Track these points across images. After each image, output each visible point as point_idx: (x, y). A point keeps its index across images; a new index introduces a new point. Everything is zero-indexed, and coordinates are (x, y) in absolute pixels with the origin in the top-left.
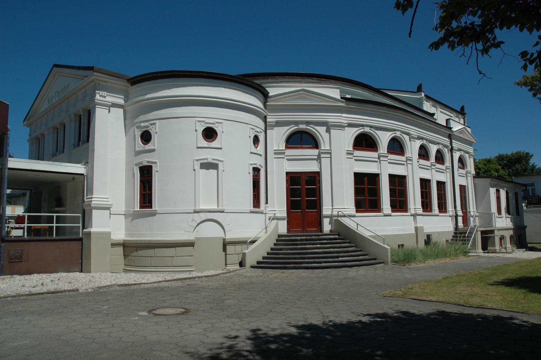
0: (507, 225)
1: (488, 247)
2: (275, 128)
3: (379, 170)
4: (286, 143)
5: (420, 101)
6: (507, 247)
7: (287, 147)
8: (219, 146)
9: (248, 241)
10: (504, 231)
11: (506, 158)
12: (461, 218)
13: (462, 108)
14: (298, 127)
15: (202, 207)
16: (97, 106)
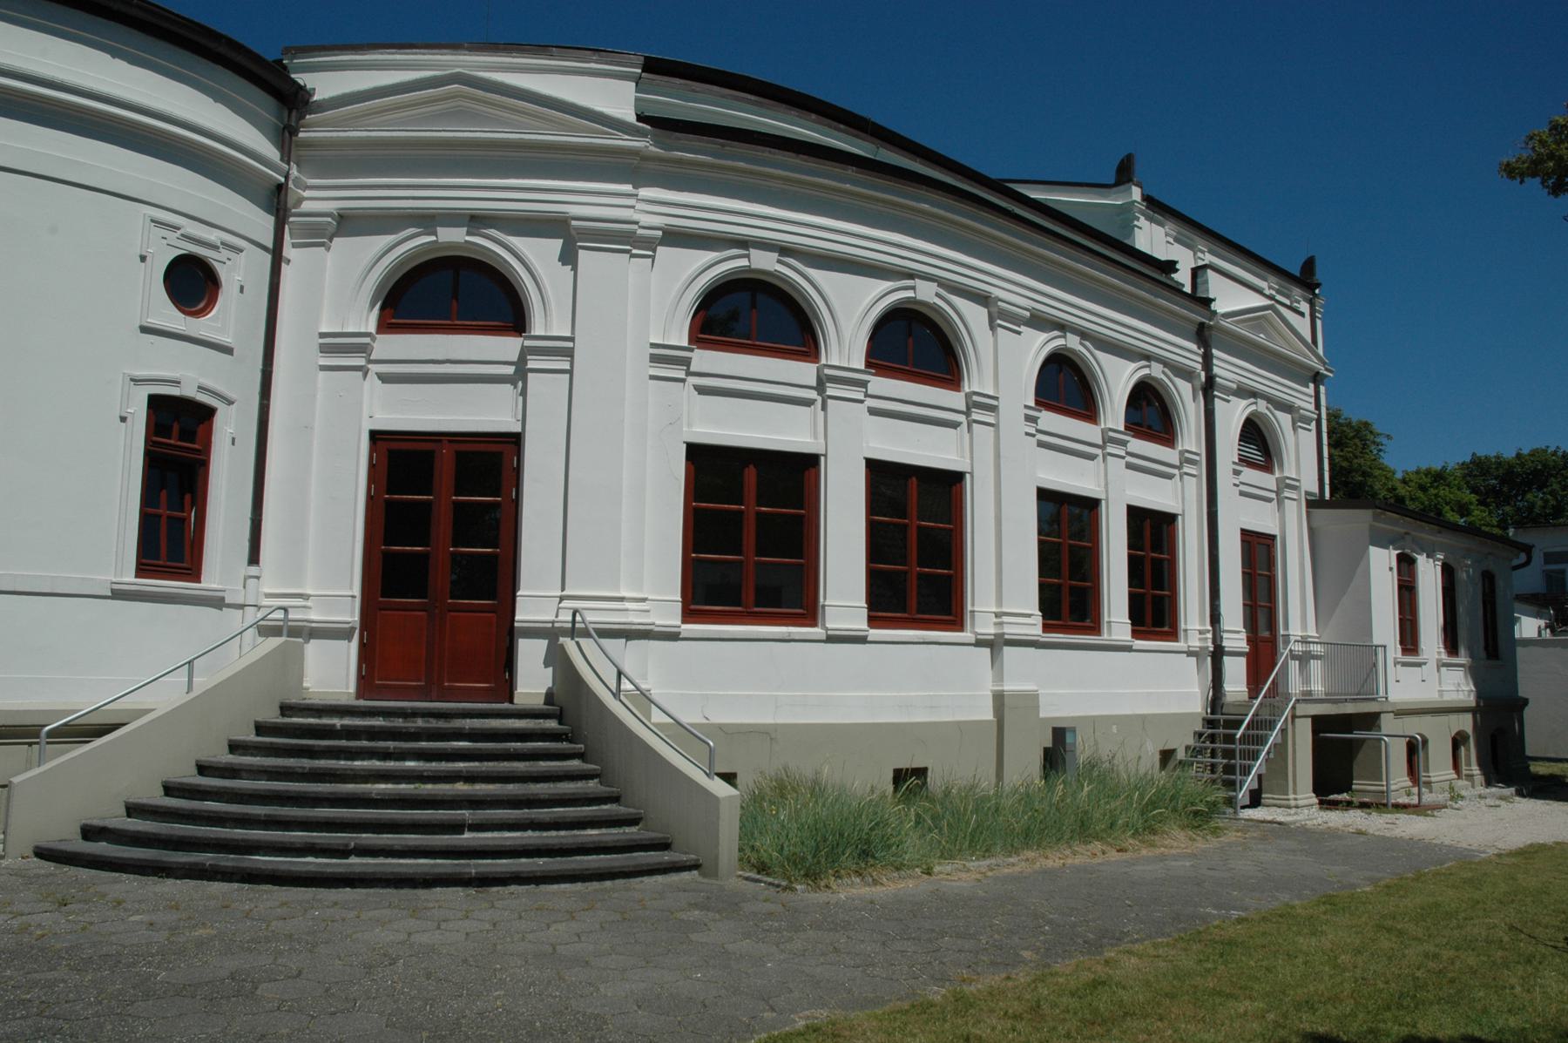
0: (1441, 696)
1: (1352, 780)
3: (816, 438)
4: (382, 309)
5: (1125, 215)
6: (1393, 787)
7: (385, 326)
9: (47, 728)
10: (1428, 718)
11: (1497, 469)
12: (1243, 661)
13: (1309, 265)
14: (433, 238)
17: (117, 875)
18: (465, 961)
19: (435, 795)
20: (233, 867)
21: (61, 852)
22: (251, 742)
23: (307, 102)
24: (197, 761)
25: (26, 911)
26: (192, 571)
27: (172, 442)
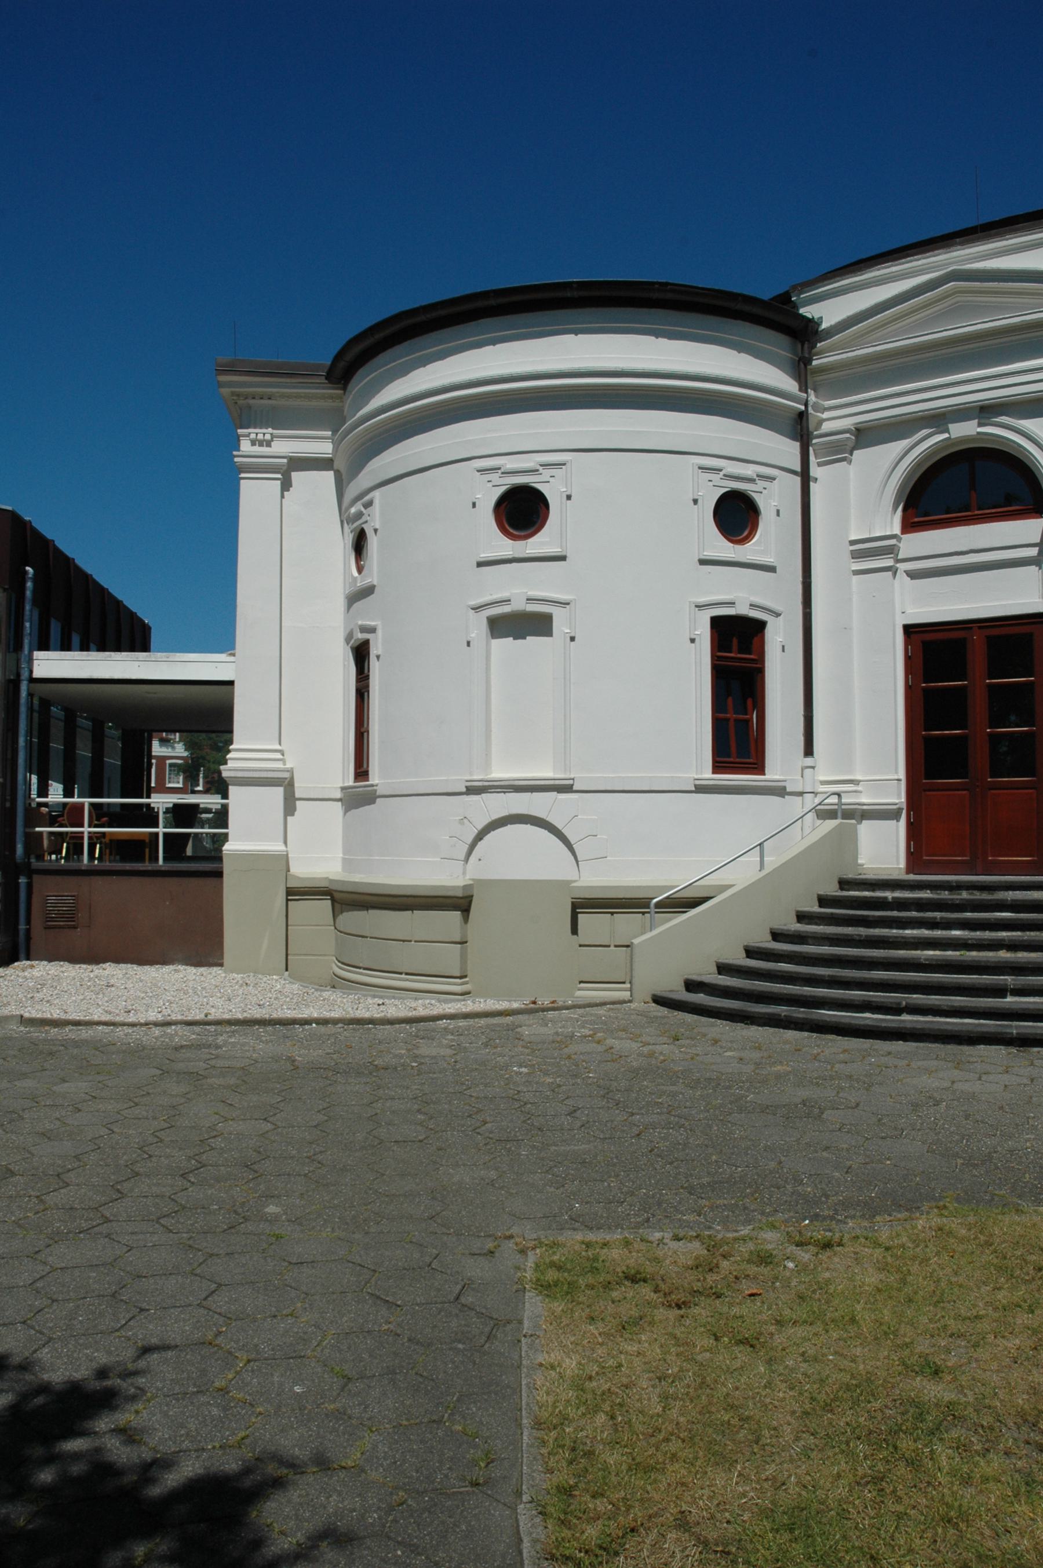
2: (857, 453)
4: (905, 510)
7: (909, 526)
8: (554, 550)
9: (655, 901)
14: (946, 435)
15: (499, 773)
16: (243, 475)
17: (713, 1020)
18: (1001, 1108)
19: (979, 961)
20: (804, 1018)
21: (671, 999)
22: (814, 912)
23: (816, 332)
24: (771, 929)
25: (652, 1042)
26: (758, 766)
27: (732, 655)
